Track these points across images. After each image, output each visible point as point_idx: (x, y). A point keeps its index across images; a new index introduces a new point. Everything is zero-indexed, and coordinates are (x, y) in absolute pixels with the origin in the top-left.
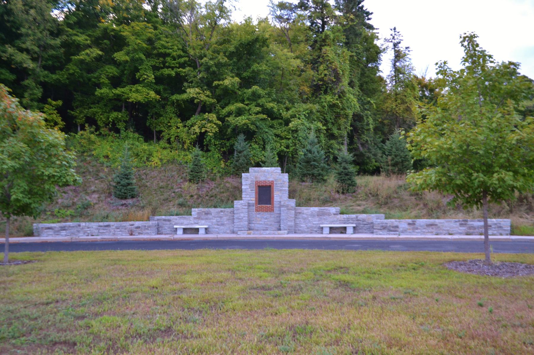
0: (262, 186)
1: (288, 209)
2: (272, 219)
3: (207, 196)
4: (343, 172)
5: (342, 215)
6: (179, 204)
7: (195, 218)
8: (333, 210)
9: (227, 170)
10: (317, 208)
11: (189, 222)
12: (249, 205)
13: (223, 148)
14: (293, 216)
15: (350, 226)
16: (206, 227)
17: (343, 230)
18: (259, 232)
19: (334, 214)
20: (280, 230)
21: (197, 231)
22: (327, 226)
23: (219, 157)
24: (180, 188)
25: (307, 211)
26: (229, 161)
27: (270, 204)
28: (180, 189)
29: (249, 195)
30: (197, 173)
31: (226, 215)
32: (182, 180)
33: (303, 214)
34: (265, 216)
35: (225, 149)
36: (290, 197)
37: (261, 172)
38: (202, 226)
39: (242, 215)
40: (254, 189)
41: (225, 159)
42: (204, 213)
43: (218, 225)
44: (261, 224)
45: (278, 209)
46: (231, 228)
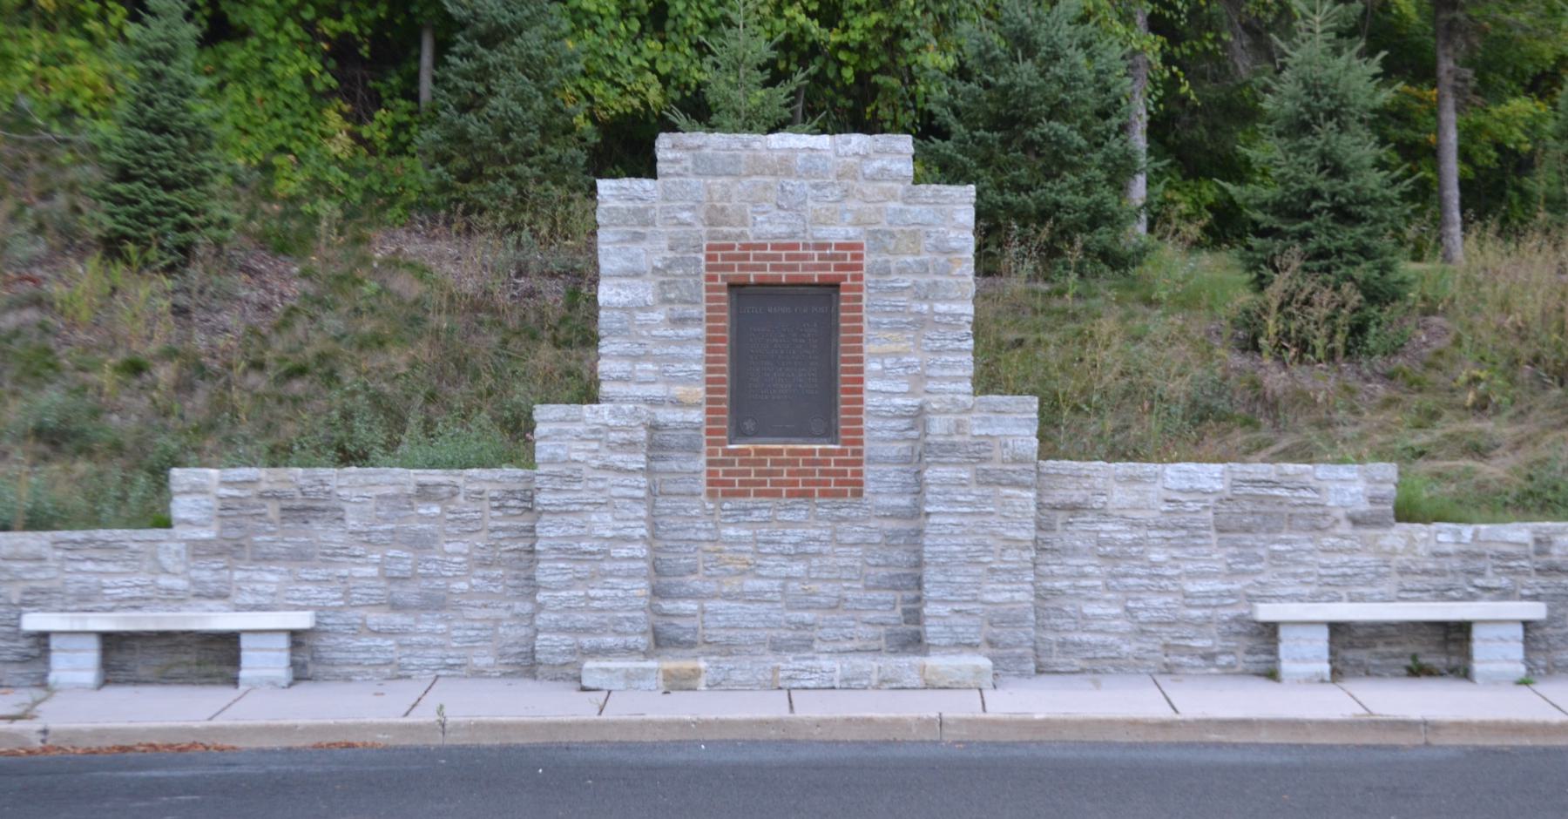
0: (768, 289)
1: (987, 479)
2: (849, 557)
3: (258, 366)
4: (1315, 194)
5: (1420, 531)
6: (40, 433)
7: (199, 550)
8: (1348, 484)
9: (373, 180)
10: (1216, 468)
11: (144, 578)
12: (658, 442)
13: (338, 16)
14: (1027, 534)
15: (1496, 617)
16: (302, 620)
17: (1445, 649)
18: (742, 667)
19: (1356, 521)
20: (913, 642)
21: (217, 656)
22: (1303, 612)
23: (307, 78)
24: (38, 302)
25: (1106, 481)
26: (380, 114)
27: (830, 434)
28: (31, 315)
29: (655, 354)
30: (168, 186)
31: (466, 527)
32: (40, 248)
33: (1104, 514)
34: (793, 536)
35: (348, 24)
36: (988, 381)
37: (758, 166)
38: (261, 614)
39: (603, 523)
40: (699, 311)
41: (349, 96)
42: (272, 509)
43: (396, 606)
44: (757, 597)
45: (893, 474)
46: (514, 633)
